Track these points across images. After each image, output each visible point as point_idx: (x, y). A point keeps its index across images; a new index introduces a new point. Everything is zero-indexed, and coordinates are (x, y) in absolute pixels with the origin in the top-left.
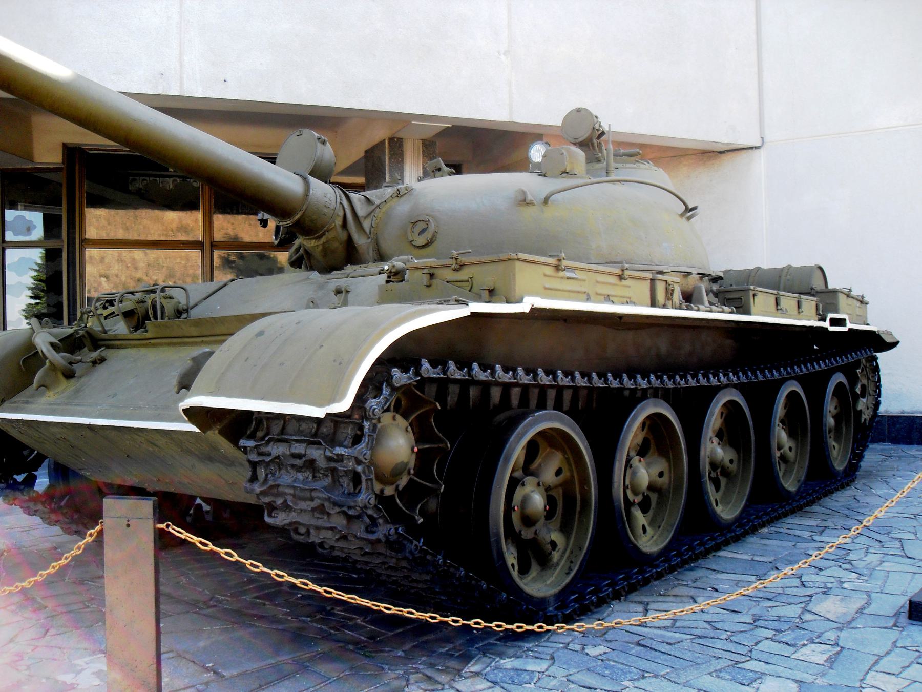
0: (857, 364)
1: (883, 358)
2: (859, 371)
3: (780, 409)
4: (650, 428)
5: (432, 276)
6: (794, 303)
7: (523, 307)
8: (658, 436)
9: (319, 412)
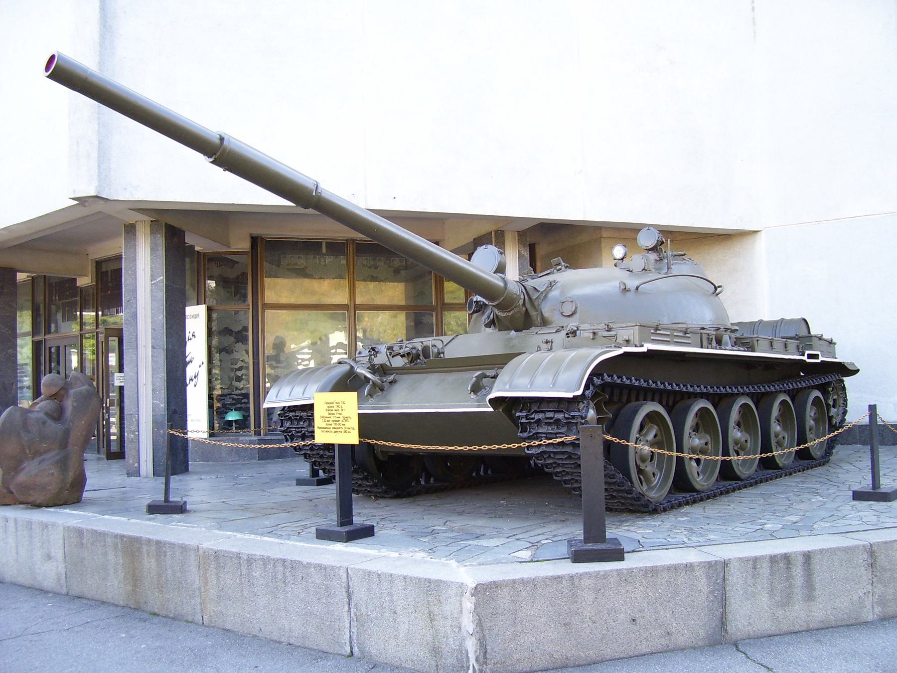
0: (829, 384)
1: (847, 381)
2: (830, 389)
3: (775, 412)
4: (700, 416)
5: (594, 333)
6: (782, 345)
7: (644, 349)
8: (704, 422)
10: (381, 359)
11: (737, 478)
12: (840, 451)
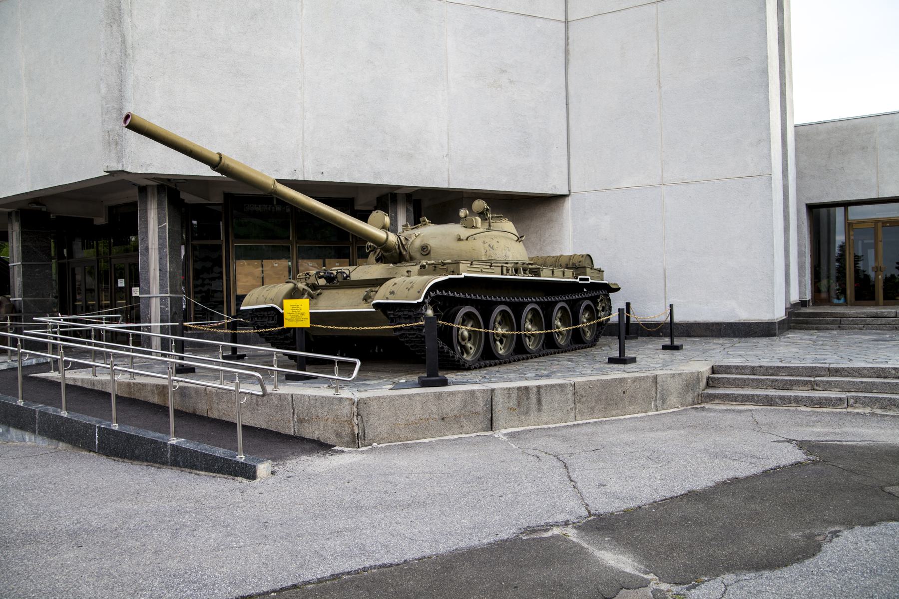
1: (611, 295)
7: (462, 276)
8: (505, 320)
9: (416, 302)
10: (312, 280)
11: (527, 352)
12: (602, 340)
